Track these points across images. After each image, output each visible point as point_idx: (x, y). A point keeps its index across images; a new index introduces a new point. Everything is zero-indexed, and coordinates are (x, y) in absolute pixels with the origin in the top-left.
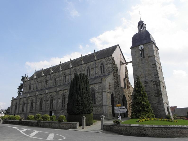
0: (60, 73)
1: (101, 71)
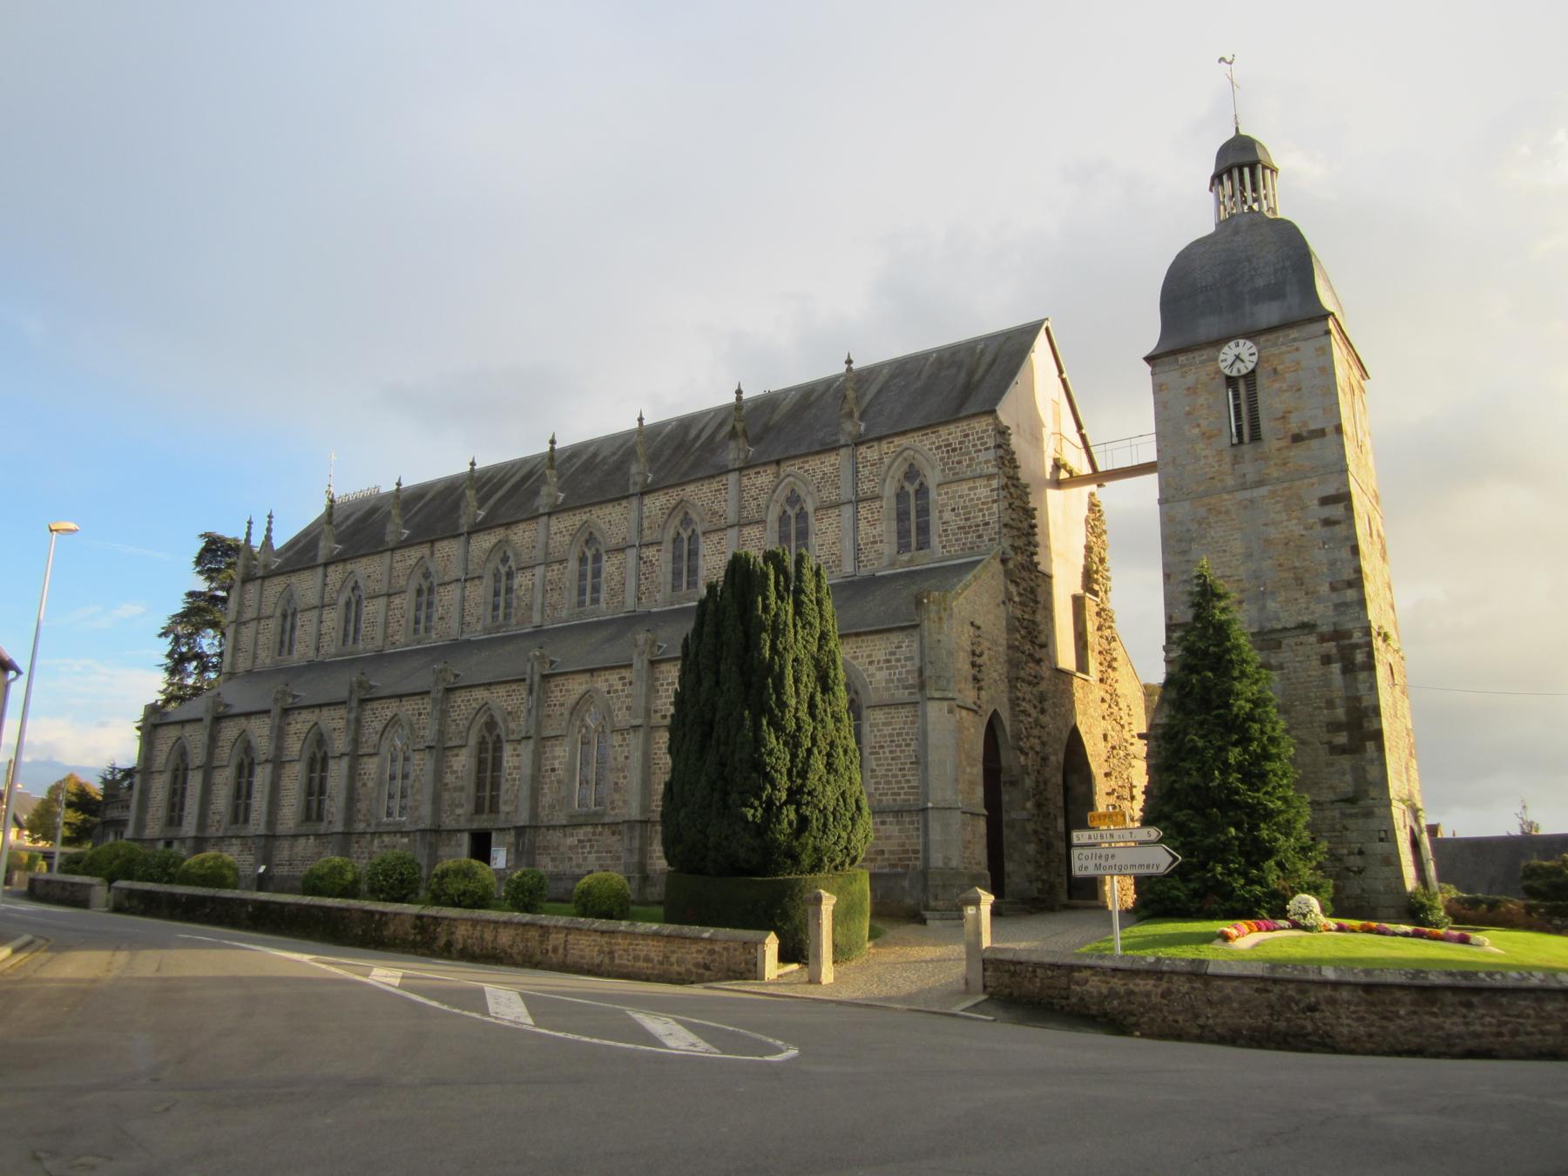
0: (553, 529)
1: (903, 534)
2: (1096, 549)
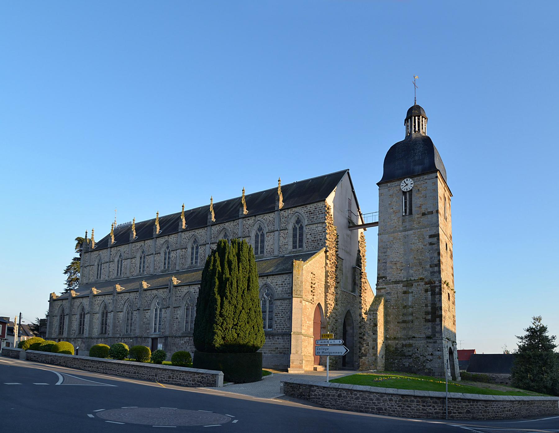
2: (361, 252)
